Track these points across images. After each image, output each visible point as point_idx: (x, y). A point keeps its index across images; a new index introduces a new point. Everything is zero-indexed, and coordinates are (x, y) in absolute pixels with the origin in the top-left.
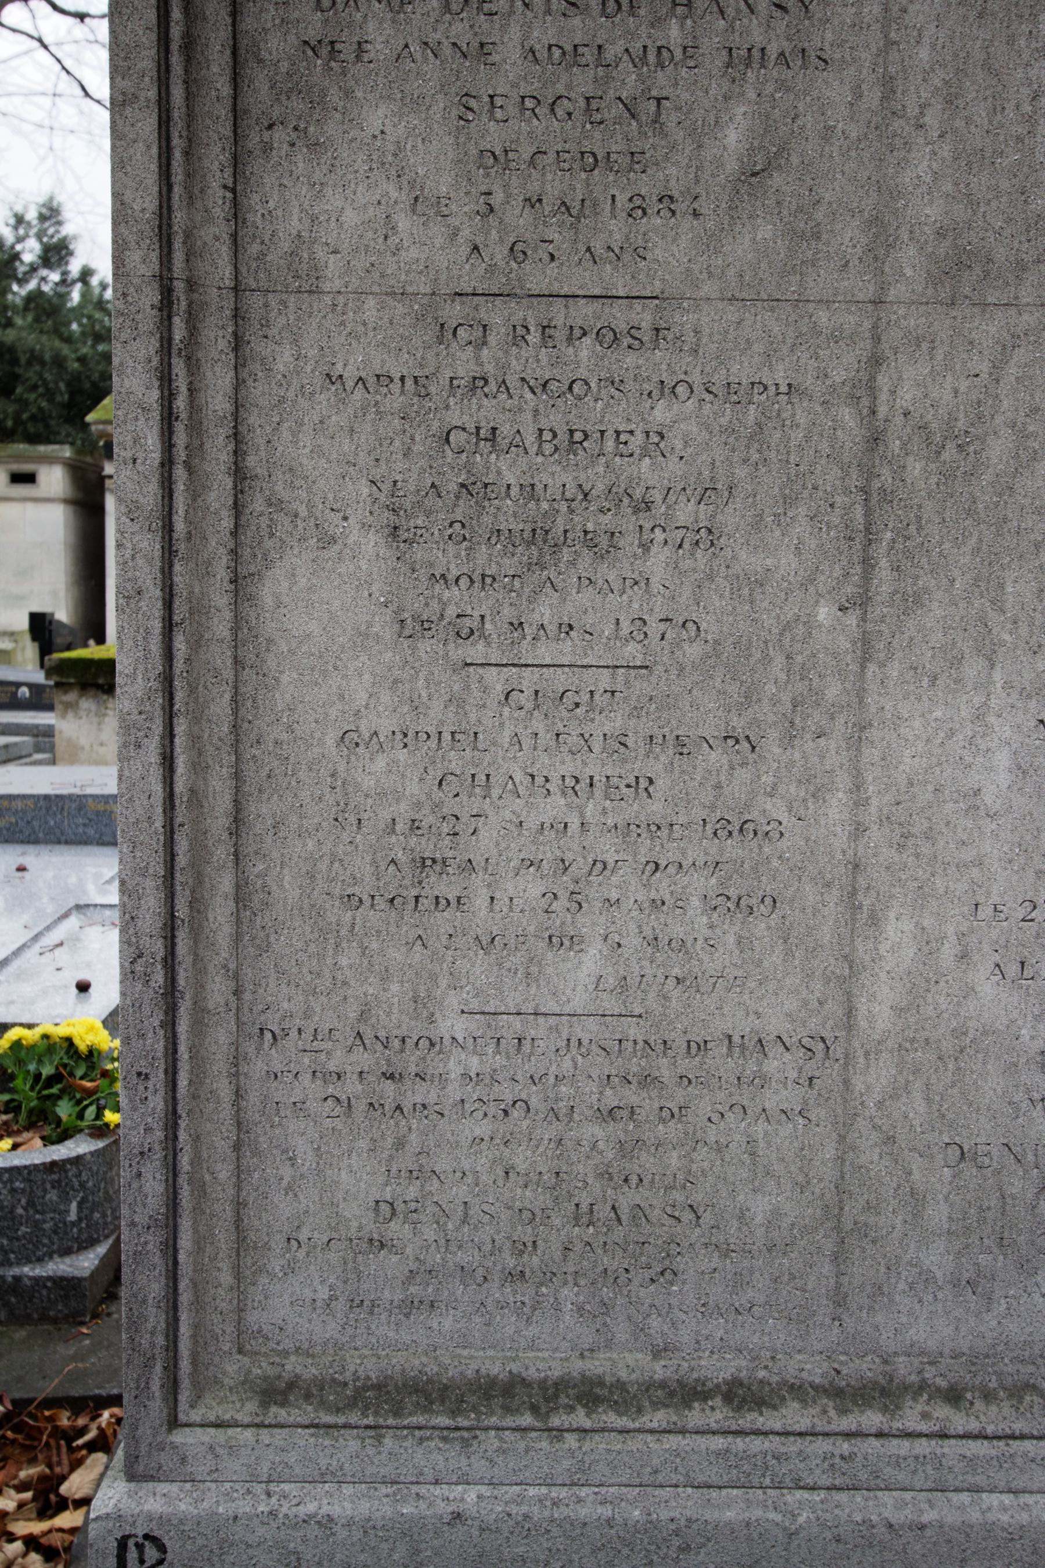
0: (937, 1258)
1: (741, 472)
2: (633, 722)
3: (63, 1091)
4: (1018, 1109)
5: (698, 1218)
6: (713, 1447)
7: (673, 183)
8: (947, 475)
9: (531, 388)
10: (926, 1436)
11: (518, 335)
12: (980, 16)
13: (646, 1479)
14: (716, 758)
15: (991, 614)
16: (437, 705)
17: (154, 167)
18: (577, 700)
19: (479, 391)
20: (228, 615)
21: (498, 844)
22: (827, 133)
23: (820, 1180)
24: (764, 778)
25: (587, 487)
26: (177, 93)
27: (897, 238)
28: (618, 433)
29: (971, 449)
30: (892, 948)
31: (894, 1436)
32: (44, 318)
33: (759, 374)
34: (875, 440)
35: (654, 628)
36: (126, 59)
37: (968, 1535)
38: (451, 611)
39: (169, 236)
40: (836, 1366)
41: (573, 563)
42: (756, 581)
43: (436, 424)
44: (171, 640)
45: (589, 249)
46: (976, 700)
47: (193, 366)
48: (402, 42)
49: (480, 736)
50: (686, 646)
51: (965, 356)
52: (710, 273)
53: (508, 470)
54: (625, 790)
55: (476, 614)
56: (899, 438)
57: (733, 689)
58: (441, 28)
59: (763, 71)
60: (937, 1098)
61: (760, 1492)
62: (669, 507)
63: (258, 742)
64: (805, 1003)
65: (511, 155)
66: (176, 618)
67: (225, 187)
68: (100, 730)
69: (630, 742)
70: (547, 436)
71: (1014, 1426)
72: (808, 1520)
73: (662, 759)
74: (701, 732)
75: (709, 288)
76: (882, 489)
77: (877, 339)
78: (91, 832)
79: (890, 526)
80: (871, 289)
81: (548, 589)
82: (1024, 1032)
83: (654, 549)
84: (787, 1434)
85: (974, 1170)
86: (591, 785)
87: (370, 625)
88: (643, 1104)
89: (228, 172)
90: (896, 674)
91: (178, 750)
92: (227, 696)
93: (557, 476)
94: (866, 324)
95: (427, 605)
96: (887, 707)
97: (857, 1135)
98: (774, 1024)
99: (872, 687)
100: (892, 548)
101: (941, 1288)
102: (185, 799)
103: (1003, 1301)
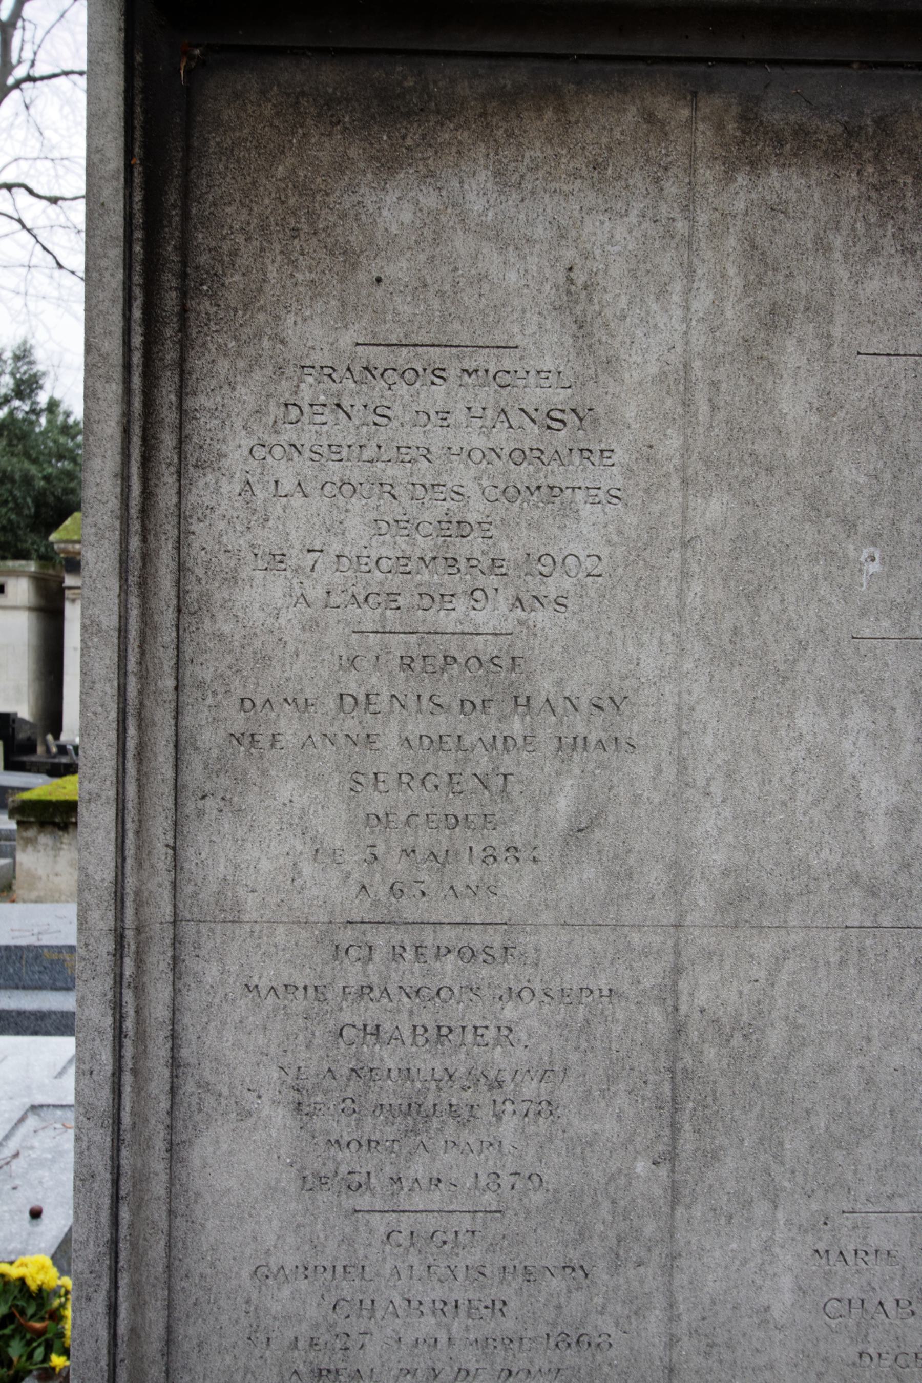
1: (573, 1057)
2: (489, 1256)
3: (15, 1331)
7: (517, 837)
9: (407, 994)
11: (397, 953)
12: (751, 713)
14: (556, 1283)
15: (774, 1166)
16: (332, 1245)
17: (112, 848)
18: (445, 1238)
19: (366, 997)
20: (164, 1177)
21: (381, 1356)
22: (636, 800)
24: (595, 1300)
25: (451, 1071)
26: (131, 790)
27: (691, 878)
28: (476, 1028)
29: (754, 1037)
32: (15, 442)
34: (678, 1030)
35: (506, 1180)
36: (92, 768)
38: (344, 1169)
39: (122, 895)
41: (440, 1130)
43: (332, 1022)
44: (117, 1208)
45: (452, 887)
46: (764, 1234)
47: (139, 990)
48: (307, 734)
49: (367, 1269)
51: (747, 966)
52: (547, 905)
53: (388, 1058)
54: (484, 1311)
55: (364, 1171)
57: (569, 1228)
58: (337, 723)
59: (585, 754)
62: (516, 1086)
63: (187, 1276)
65: (391, 817)
66: (122, 1193)
67: (167, 846)
68: (55, 862)
69: (487, 1272)
70: (420, 1031)
73: (513, 1285)
74: (544, 1263)
75: (546, 917)
76: (685, 1069)
77: (677, 954)
78: (46, 978)
80: (673, 916)
81: (421, 1150)
83: (505, 1118)
86: (456, 1307)
87: (278, 1181)
89: (170, 834)
91: (121, 1299)
92: (162, 1243)
93: (427, 1062)
95: (324, 1164)
102: (126, 1339)
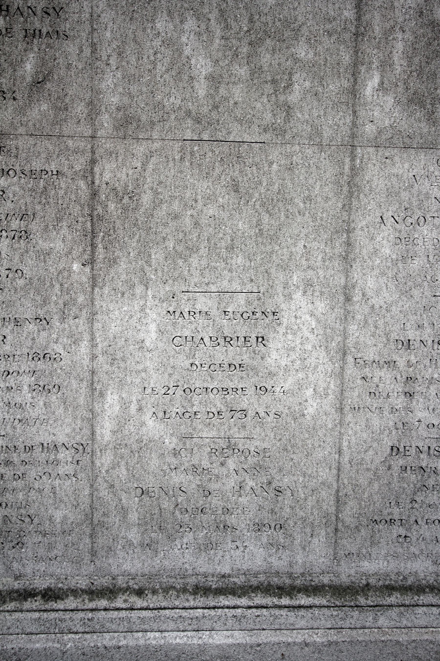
0: (134, 535)
1: (38, 207)
4: (165, 472)
5: (32, 520)
6: (34, 617)
8: (125, 209)
10: (125, 609)
12: (131, 19)
13: (5, 632)
14: (32, 327)
15: (146, 267)
22: (69, 66)
23: (83, 503)
24: (53, 336)
27: (100, 111)
29: (135, 198)
30: (110, 406)
31: (111, 610)
33: (44, 167)
34: (94, 194)
37: (138, 650)
40: (92, 581)
42: (46, 253)
50: (17, 280)
56: (104, 194)
57: (38, 298)
59: (40, 40)
60: (131, 469)
61: (54, 635)
62: (8, 222)
64: (74, 429)
71: (162, 604)
72: (71, 647)
74: (25, 316)
75: (21, 130)
76: (98, 215)
77: (93, 152)
79: (102, 230)
80: (90, 131)
82: (166, 440)
84: (66, 610)
85: (148, 499)
88: (6, 473)
90: (107, 292)
94: (88, 146)
96: (104, 306)
97: (98, 484)
98: (61, 438)
99: (97, 297)
100: (103, 239)
101: (136, 548)
103: (162, 552)
